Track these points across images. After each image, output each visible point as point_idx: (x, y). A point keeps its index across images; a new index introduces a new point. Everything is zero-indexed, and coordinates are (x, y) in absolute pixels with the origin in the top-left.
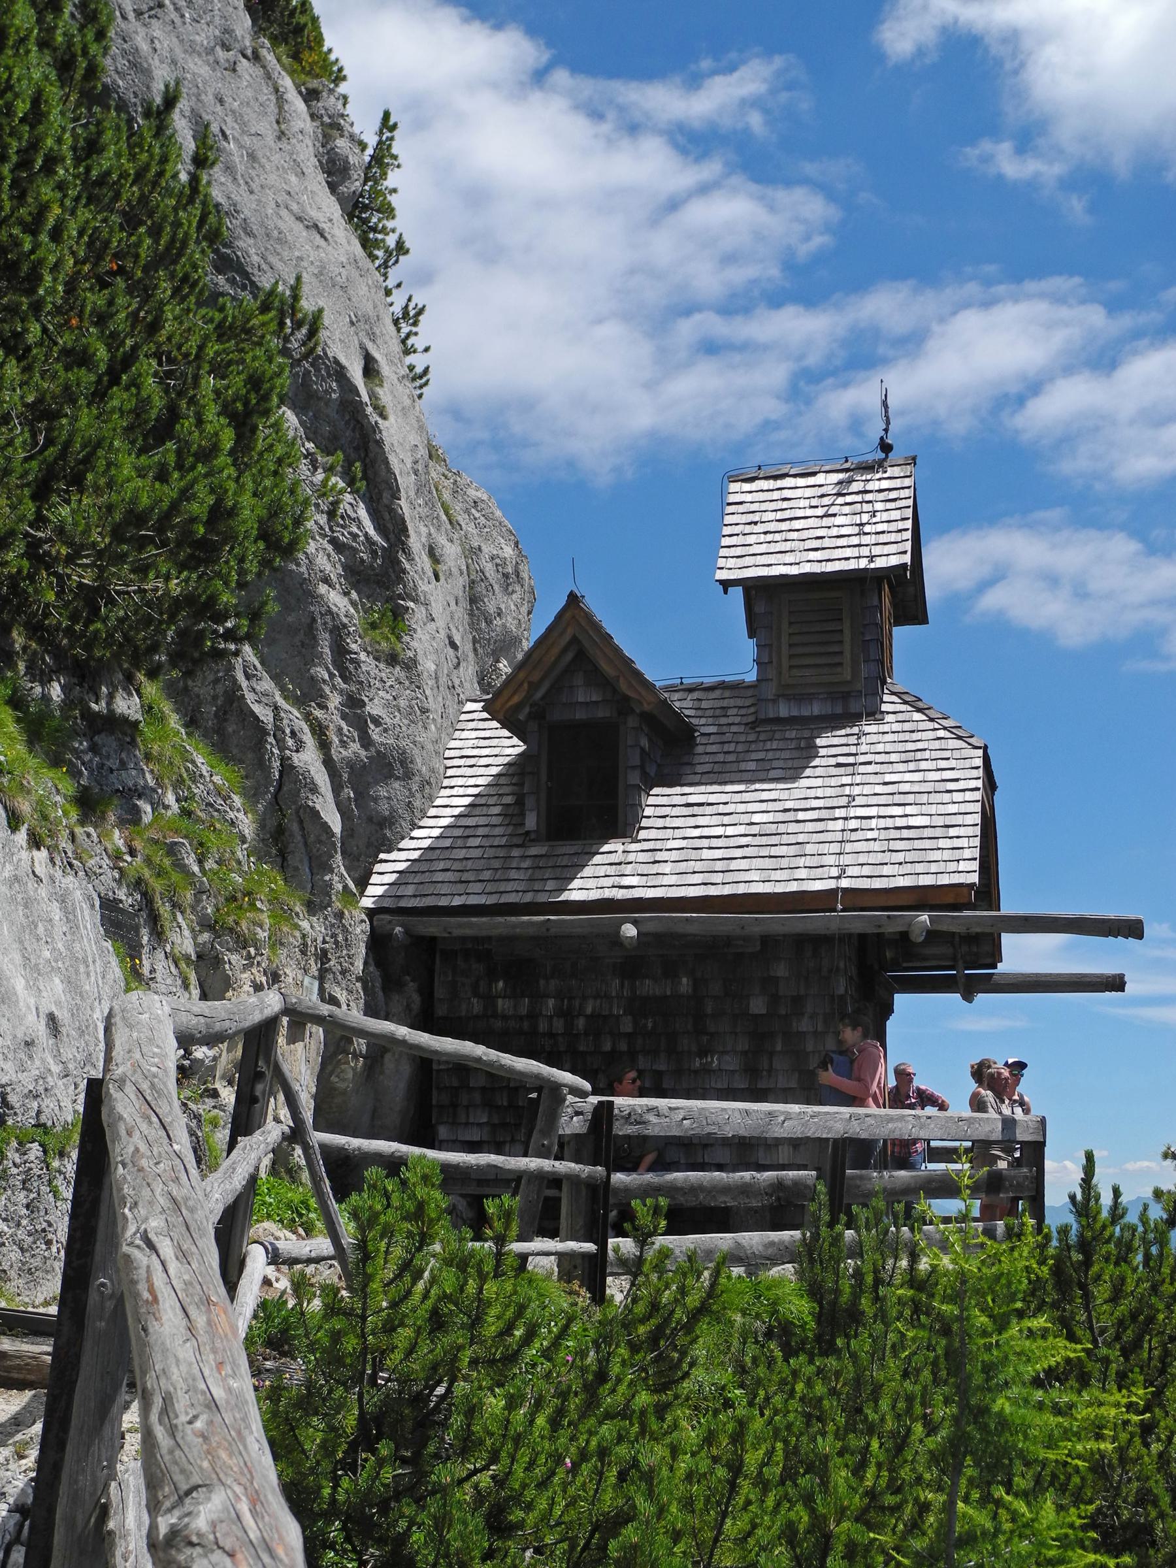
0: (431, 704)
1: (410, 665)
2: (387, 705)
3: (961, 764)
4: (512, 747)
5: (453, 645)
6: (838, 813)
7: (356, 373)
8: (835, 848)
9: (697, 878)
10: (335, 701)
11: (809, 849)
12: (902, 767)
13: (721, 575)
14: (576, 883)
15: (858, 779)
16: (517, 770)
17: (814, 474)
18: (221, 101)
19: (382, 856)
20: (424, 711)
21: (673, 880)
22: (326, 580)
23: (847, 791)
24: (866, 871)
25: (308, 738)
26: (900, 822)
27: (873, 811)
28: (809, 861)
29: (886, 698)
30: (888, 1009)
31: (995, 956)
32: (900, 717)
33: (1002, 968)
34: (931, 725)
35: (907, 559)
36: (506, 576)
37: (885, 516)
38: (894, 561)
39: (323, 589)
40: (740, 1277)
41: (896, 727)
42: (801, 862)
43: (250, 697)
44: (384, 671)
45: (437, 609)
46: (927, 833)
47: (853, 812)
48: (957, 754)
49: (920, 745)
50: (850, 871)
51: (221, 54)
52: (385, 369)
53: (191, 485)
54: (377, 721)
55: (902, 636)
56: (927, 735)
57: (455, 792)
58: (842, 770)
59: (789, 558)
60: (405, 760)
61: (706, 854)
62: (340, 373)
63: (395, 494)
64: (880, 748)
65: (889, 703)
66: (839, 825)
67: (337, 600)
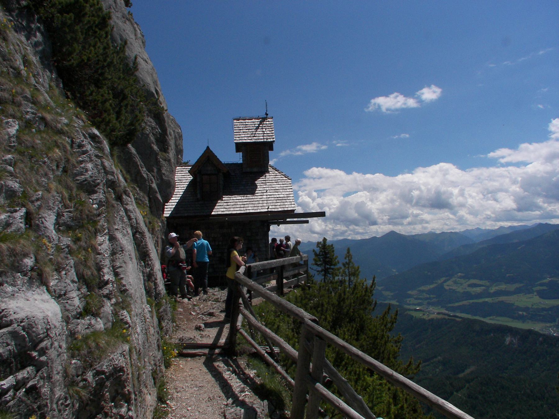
1: (169, 161)
2: (166, 170)
3: (287, 183)
6: (265, 194)
9: (238, 209)
10: (155, 170)
12: (275, 184)
14: (214, 210)
15: (267, 186)
17: (252, 119)
19: (166, 204)
22: (153, 143)
23: (265, 189)
26: (278, 196)
27: (272, 194)
28: (261, 205)
29: (269, 168)
32: (273, 172)
34: (279, 174)
37: (268, 130)
40: (59, 269)
41: (272, 174)
42: (259, 205)
43: (142, 172)
46: (284, 198)
48: (286, 181)
49: (278, 179)
50: (270, 207)
51: (123, 19)
52: (160, 93)
54: (164, 174)
57: (179, 188)
58: (263, 184)
61: (238, 203)
64: (270, 179)
65: (270, 169)
66: (265, 197)
67: (155, 147)
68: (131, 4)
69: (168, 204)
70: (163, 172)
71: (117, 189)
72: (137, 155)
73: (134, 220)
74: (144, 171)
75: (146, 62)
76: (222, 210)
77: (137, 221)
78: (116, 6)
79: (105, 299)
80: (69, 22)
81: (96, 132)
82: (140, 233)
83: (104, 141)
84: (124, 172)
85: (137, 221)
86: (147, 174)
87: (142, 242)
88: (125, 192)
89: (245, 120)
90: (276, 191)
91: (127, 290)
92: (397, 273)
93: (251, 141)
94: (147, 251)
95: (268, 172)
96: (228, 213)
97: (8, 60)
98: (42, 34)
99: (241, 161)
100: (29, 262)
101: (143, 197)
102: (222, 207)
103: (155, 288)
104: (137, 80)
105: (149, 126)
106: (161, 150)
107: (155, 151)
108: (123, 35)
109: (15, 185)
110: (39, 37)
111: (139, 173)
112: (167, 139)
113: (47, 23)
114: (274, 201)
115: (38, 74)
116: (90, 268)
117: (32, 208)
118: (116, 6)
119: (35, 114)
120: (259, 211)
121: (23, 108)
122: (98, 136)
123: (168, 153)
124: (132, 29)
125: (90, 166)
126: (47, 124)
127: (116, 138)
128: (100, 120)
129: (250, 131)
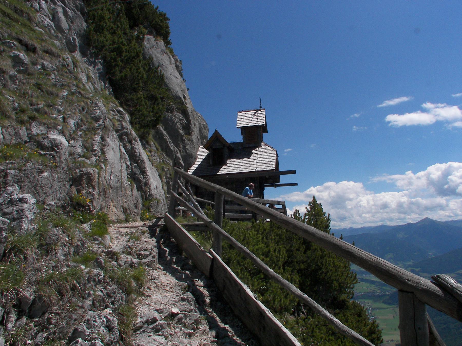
0: (195, 147)
1: (192, 141)
2: (189, 147)
4: (207, 152)
5: (198, 138)
7: (183, 99)
8: (255, 165)
10: (181, 146)
11: (252, 165)
13: (237, 126)
14: (219, 172)
16: (208, 156)
18: (162, 60)
20: (194, 148)
21: (232, 171)
24: (260, 168)
25: (179, 152)
27: (260, 160)
30: (264, 189)
31: (279, 181)
33: (280, 183)
35: (264, 123)
36: (205, 127)
38: (262, 124)
39: (179, 130)
42: (250, 167)
43: (170, 146)
44: (188, 142)
45: (195, 132)
47: (258, 160)
51: (162, 53)
52: (187, 98)
53: (117, 110)
54: (188, 149)
55: (264, 135)
56: (268, 149)
59: (247, 124)
60: (192, 155)
61: (237, 167)
62: (180, 98)
63: (189, 116)
65: (262, 144)
66: (256, 162)
67: (181, 132)
68: (171, 43)
69: (191, 169)
70: (187, 147)
71: (129, 137)
72: (167, 136)
73: (138, 153)
74: (172, 146)
75: (177, 78)
76: (225, 171)
77: (140, 154)
78: (157, 46)
79: (93, 156)
80: (113, 57)
81: (121, 109)
82: (141, 160)
83: (126, 115)
84: (157, 145)
85: (140, 154)
86: (174, 148)
87: (142, 165)
88: (135, 140)
89: (246, 112)
90: (264, 158)
91: (107, 159)
92: (433, 256)
93: (248, 125)
94: (145, 171)
95: (261, 146)
96: (228, 173)
97: (73, 73)
98: (101, 64)
99: (242, 141)
100: (60, 127)
101: (168, 160)
102: (226, 169)
103: (149, 191)
104: (168, 89)
105: (178, 118)
106: (186, 134)
107: (181, 134)
108: (161, 63)
109: (61, 109)
110: (100, 66)
111: (168, 146)
112: (190, 127)
113: (104, 58)
114: (261, 165)
115: (95, 83)
116: (88, 143)
117: (66, 117)
118: (157, 46)
119: (76, 90)
120: (249, 171)
121: (72, 88)
122: (122, 111)
123: (192, 136)
124: (168, 58)
125: (98, 111)
126: (82, 95)
127: (147, 121)
128: (135, 109)
129: (248, 119)
